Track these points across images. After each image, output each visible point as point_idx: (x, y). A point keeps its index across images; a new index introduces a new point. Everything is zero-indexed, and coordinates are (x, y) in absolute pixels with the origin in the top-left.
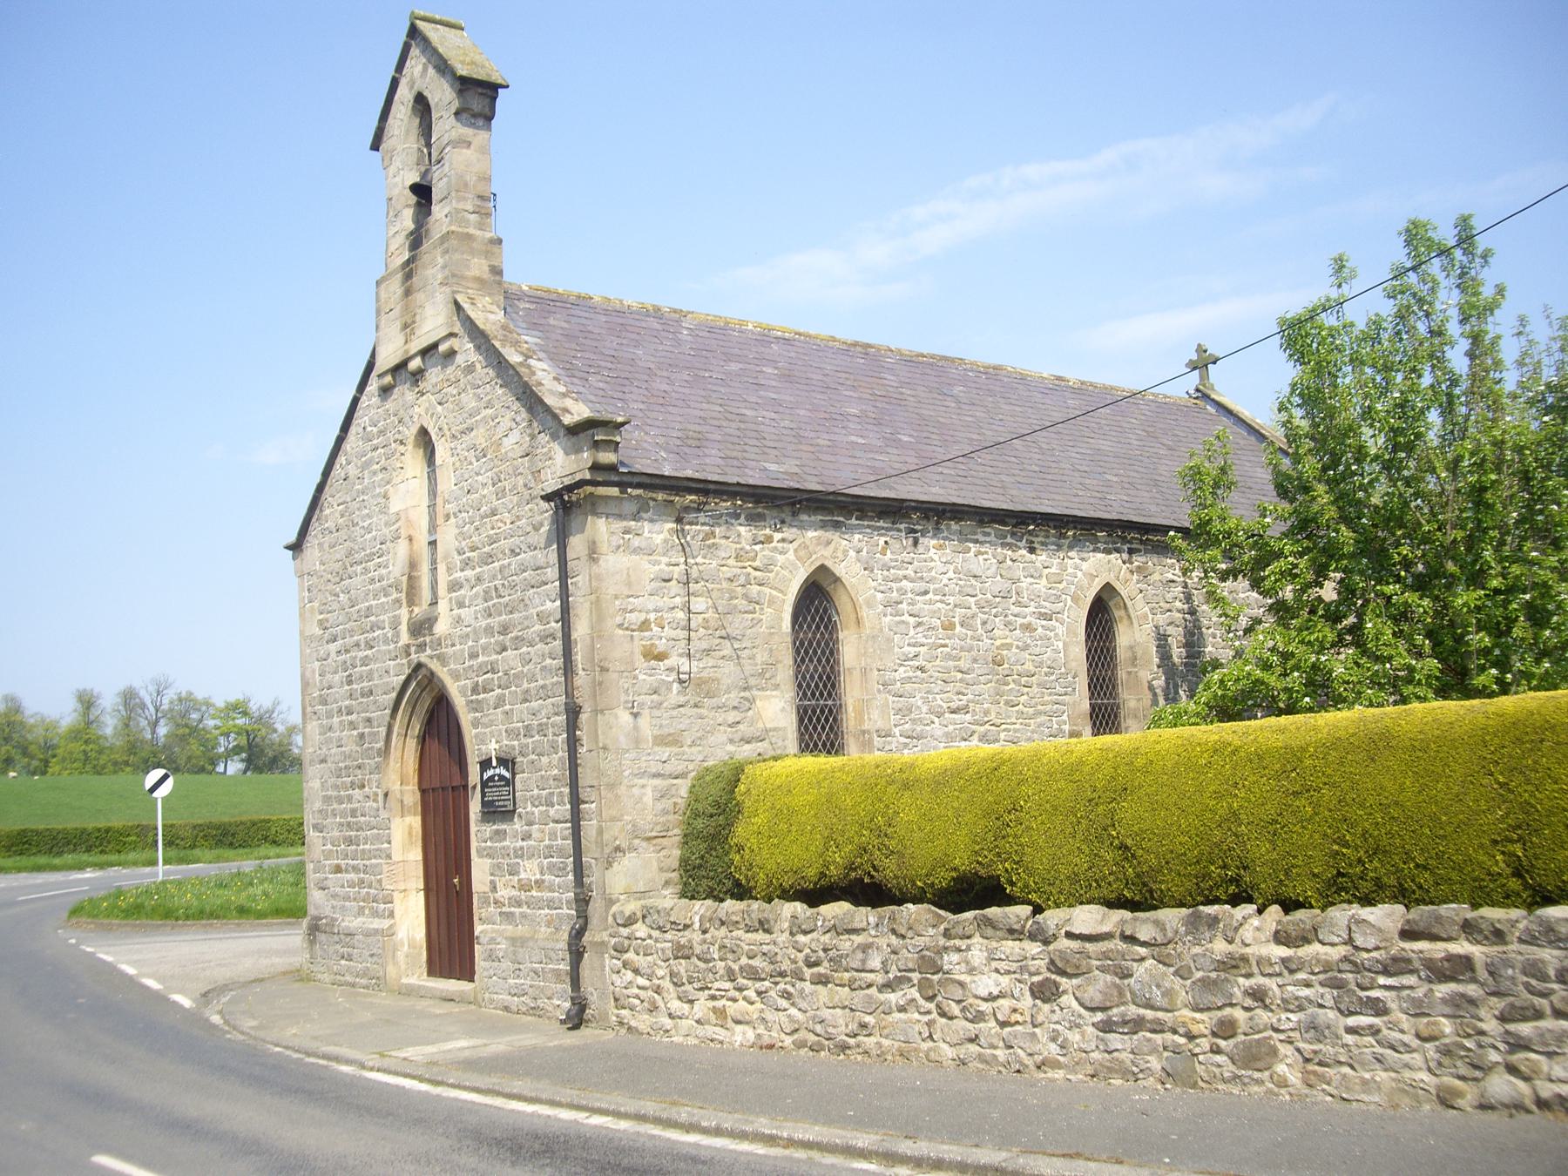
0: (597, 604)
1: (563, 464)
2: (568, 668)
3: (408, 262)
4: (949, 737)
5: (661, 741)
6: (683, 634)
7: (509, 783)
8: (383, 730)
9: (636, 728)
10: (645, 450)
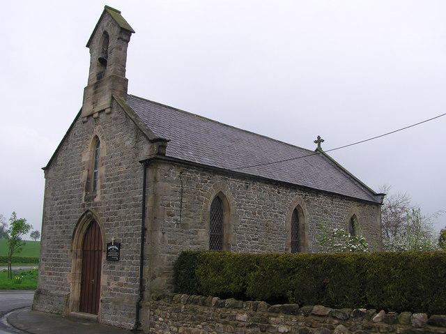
0: (155, 195)
1: (146, 151)
2: (144, 216)
3: (96, 83)
4: (252, 248)
5: (170, 242)
6: (179, 209)
7: (118, 251)
8: (72, 231)
9: (163, 237)
10: (170, 152)
